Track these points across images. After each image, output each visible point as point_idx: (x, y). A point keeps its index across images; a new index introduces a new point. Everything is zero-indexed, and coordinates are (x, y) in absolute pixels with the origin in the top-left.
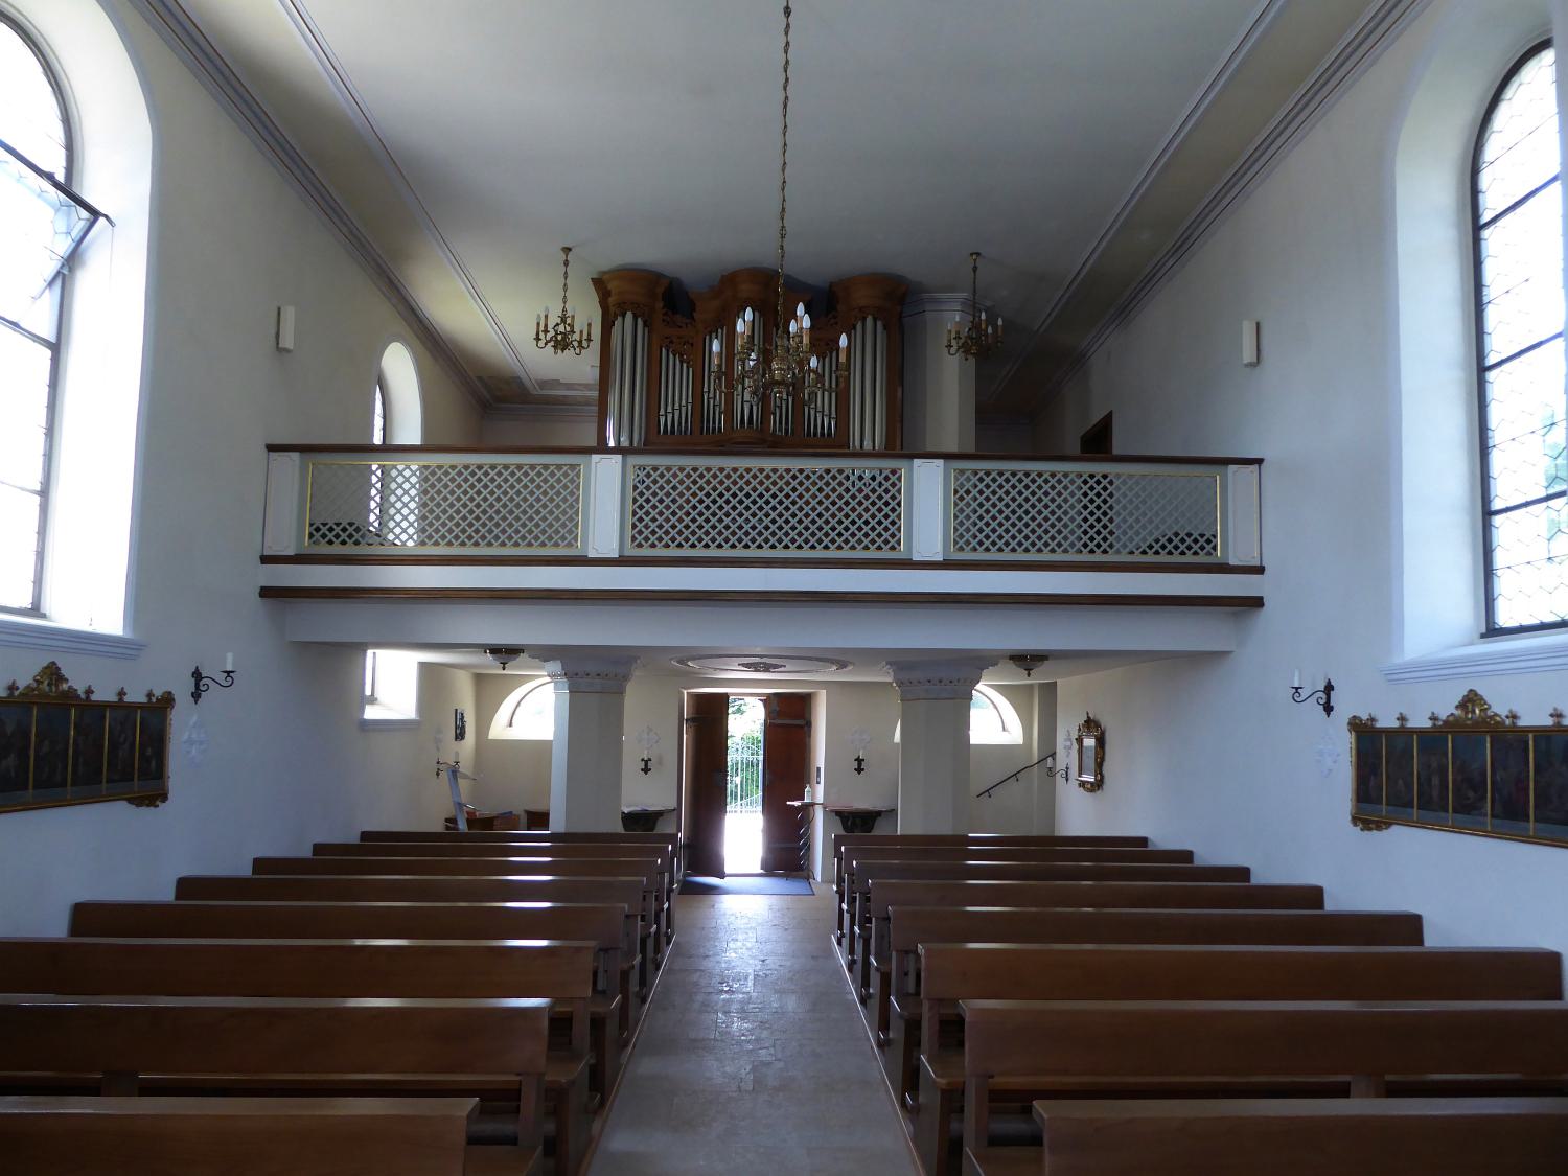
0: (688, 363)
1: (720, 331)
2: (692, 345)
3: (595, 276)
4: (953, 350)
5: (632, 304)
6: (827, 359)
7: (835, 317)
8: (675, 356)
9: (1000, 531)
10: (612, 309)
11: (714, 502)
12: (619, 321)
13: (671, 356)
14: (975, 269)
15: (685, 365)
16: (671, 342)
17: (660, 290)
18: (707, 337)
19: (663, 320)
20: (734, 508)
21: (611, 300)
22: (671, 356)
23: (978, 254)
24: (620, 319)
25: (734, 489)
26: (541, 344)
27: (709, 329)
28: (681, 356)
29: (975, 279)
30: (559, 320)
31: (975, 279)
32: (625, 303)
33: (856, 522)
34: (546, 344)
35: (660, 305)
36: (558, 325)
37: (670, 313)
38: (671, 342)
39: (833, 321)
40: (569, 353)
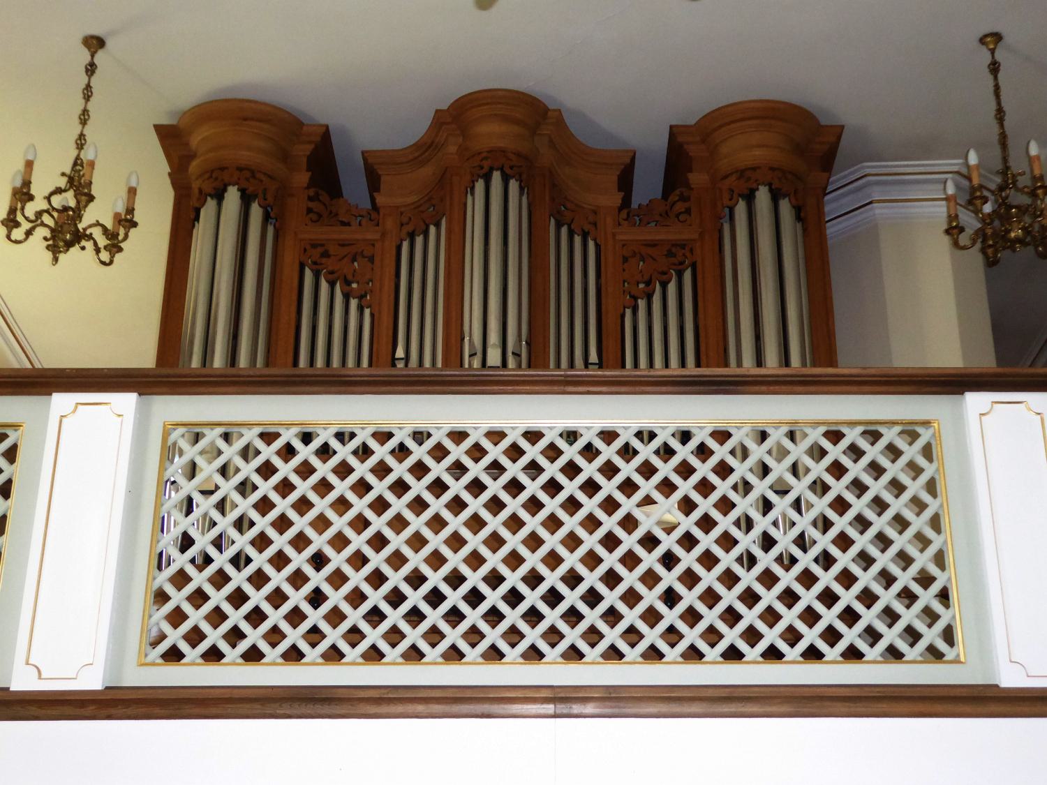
0: (361, 298)
1: (432, 229)
2: (371, 259)
3: (164, 121)
4: (964, 239)
5: (240, 169)
6: (672, 288)
7: (683, 198)
8: (332, 285)
9: (278, 579)
10: (196, 185)
11: (396, 598)
12: (210, 207)
13: (324, 286)
14: (994, 68)
15: (354, 303)
16: (326, 254)
17: (303, 151)
18: (405, 246)
19: (309, 211)
20: (415, 616)
21: (194, 167)
22: (324, 286)
23: (997, 37)
24: (211, 204)
25: (319, 542)
26: (18, 234)
27: (410, 228)
28: (347, 283)
29: (997, 89)
30: (63, 183)
31: (997, 89)
32: (222, 169)
33: (343, 617)
34: (29, 233)
35: (302, 178)
36: (58, 191)
37: (324, 197)
38: (326, 254)
39: (680, 207)
40: (79, 258)
